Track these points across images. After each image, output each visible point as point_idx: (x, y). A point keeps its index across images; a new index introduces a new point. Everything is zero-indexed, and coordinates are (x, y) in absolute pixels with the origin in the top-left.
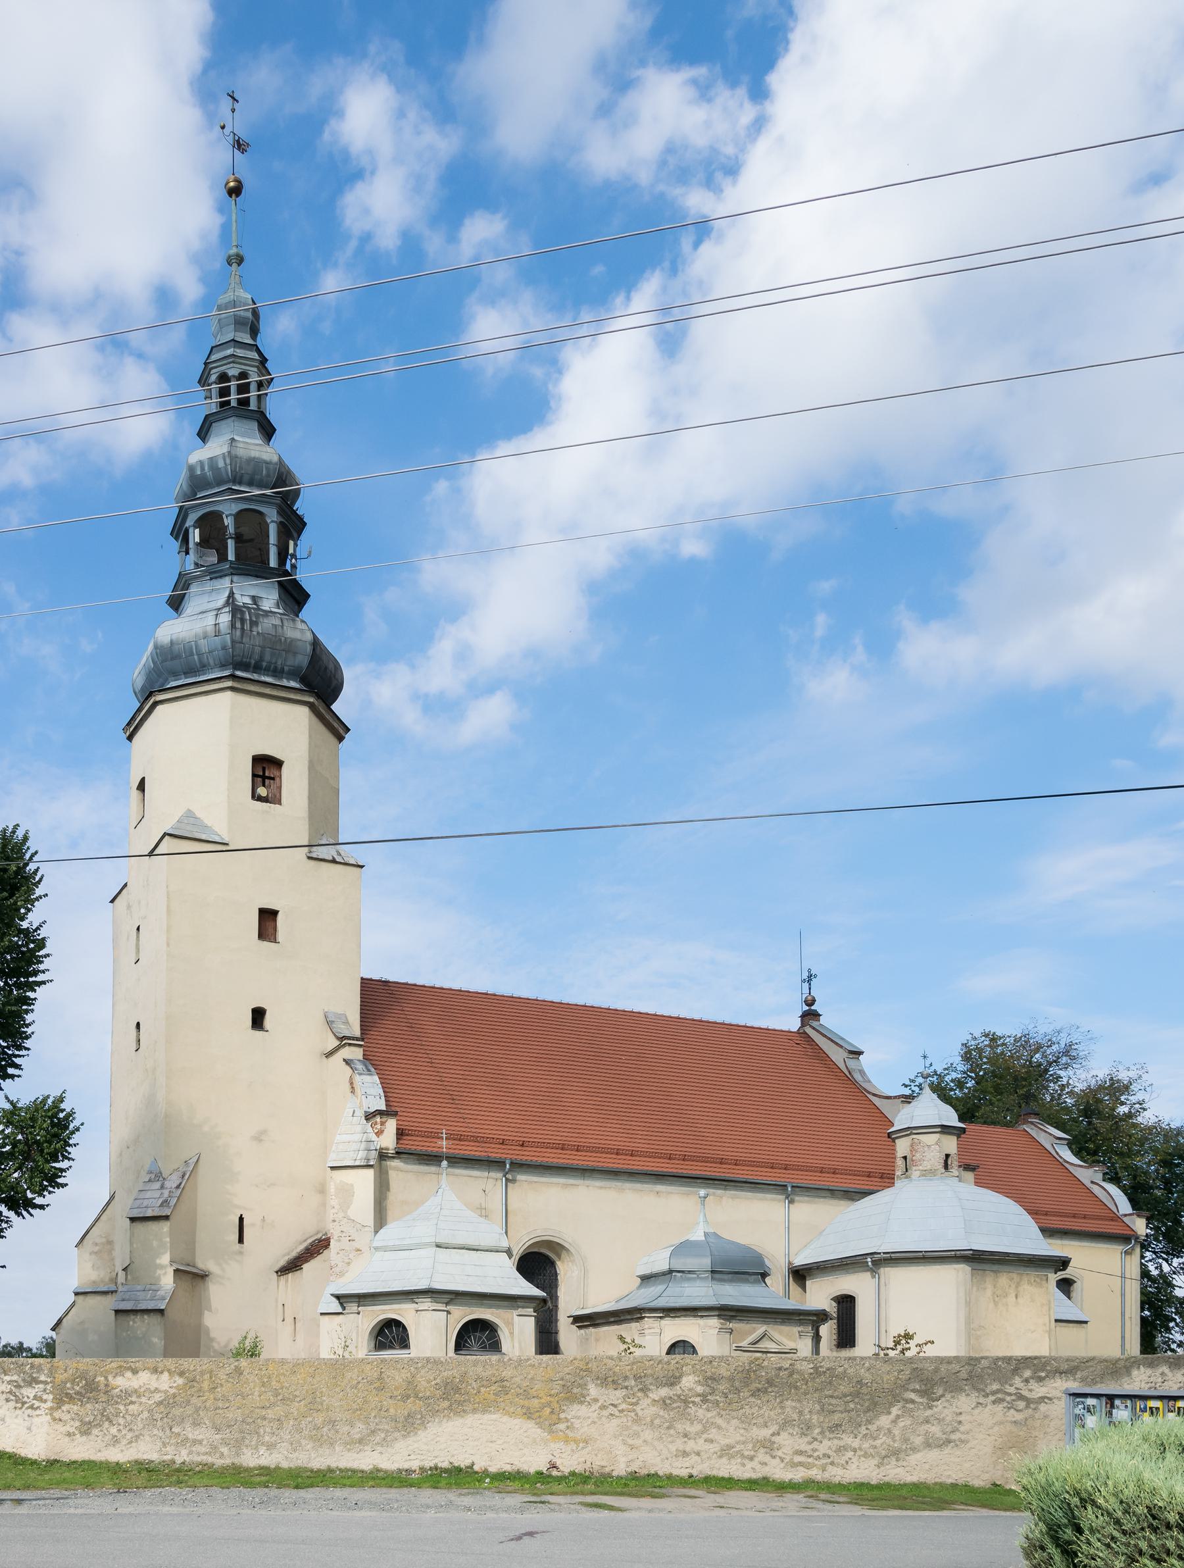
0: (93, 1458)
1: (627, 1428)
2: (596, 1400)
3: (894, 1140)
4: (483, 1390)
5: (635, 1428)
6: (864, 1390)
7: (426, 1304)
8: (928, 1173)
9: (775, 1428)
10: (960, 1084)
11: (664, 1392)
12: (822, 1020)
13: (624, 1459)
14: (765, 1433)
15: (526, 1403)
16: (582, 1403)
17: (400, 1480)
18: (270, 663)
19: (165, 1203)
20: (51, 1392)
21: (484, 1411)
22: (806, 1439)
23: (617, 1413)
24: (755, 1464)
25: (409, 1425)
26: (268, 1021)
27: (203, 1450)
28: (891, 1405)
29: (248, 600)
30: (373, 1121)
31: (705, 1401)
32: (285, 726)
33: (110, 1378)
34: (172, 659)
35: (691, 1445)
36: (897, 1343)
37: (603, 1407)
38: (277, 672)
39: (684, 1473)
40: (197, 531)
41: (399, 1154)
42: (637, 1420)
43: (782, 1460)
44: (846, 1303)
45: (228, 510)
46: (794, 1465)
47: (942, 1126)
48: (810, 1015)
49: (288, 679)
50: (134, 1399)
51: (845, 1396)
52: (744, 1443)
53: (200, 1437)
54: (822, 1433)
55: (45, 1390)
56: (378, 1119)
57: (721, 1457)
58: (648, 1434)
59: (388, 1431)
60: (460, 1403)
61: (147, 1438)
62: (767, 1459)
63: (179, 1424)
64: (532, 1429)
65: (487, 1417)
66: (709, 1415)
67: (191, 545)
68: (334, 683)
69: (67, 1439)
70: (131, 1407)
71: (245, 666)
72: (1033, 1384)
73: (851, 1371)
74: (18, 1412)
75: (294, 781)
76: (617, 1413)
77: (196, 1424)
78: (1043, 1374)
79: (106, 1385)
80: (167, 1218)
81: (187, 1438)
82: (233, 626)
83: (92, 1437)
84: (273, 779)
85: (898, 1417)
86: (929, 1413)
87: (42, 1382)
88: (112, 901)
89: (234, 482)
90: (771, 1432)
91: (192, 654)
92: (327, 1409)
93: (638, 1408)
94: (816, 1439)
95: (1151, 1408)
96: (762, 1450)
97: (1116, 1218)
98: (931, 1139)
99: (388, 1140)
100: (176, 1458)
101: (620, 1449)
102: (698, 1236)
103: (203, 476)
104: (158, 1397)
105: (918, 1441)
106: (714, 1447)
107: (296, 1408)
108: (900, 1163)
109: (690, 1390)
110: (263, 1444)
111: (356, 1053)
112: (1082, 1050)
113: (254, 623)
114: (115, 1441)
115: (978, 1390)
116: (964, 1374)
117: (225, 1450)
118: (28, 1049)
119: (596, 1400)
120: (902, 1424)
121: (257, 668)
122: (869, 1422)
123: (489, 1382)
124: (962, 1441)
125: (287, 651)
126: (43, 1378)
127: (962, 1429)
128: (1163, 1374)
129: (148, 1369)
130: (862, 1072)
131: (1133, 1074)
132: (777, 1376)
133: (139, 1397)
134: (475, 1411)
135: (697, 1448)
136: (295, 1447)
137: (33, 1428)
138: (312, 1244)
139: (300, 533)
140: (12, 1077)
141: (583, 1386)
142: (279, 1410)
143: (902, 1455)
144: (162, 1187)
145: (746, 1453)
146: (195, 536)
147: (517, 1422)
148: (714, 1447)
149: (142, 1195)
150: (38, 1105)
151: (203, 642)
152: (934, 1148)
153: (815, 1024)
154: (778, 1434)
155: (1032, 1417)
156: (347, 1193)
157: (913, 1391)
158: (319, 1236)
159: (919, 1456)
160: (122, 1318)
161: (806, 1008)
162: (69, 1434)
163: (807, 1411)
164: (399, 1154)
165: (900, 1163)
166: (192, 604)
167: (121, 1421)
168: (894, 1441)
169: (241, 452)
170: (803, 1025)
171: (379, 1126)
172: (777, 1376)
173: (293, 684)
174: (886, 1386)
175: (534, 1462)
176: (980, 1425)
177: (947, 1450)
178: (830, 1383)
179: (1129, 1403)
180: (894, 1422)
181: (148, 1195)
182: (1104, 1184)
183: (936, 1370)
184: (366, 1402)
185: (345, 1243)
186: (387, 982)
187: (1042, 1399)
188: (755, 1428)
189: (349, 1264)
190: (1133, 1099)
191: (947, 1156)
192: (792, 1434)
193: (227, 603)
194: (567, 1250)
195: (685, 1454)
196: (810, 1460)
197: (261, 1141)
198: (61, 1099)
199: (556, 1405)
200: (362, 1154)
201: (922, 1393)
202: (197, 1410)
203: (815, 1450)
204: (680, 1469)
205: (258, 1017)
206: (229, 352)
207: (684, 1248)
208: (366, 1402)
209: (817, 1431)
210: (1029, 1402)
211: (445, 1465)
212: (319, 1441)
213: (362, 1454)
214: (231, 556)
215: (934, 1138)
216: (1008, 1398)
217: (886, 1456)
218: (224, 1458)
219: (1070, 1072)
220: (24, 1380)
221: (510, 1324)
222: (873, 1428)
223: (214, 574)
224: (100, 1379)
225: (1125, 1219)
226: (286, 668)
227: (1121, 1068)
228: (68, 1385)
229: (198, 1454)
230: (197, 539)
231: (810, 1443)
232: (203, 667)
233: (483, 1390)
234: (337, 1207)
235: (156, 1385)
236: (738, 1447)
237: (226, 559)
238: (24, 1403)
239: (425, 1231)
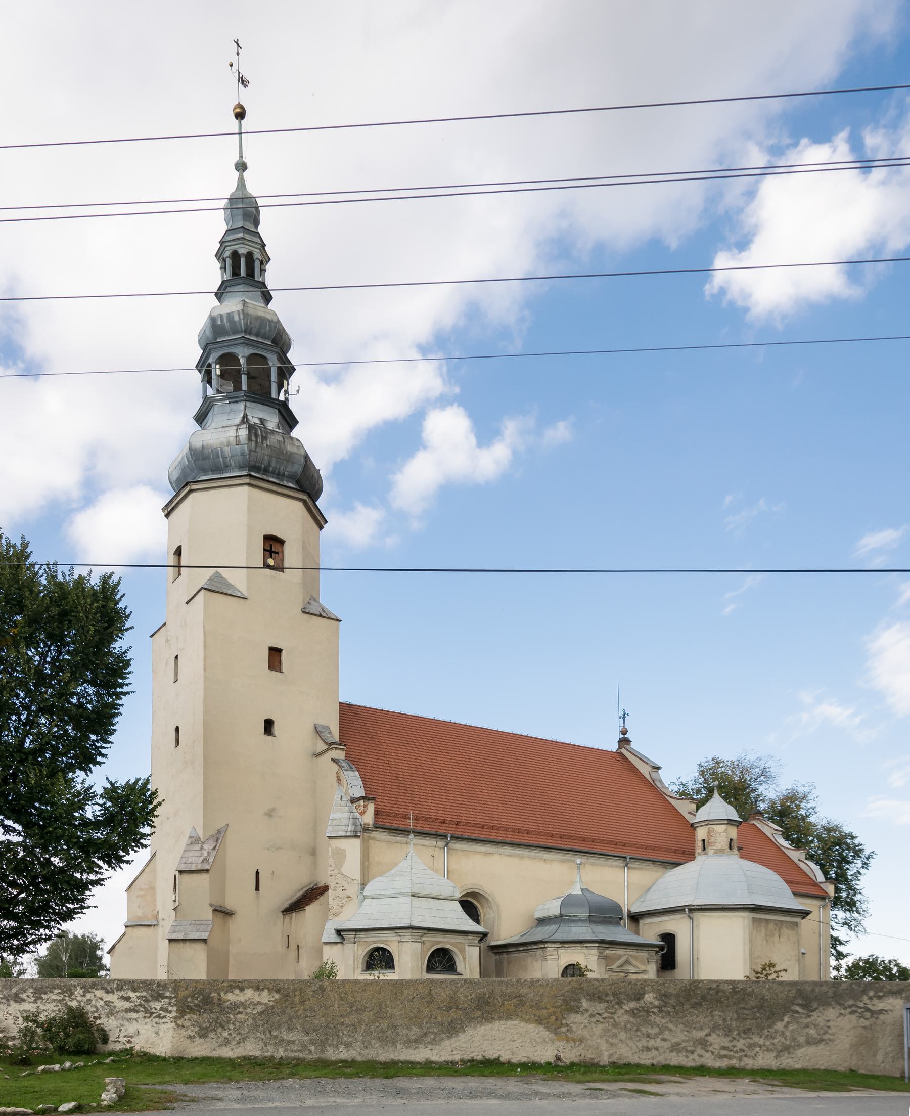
0: (209, 1055)
1: (609, 1030)
2: (587, 1010)
3: (695, 829)
4: (506, 1003)
5: (614, 1030)
6: (766, 1004)
7: (407, 936)
8: (719, 852)
9: (707, 1031)
10: (698, 791)
11: (633, 1005)
12: (633, 745)
13: (606, 1053)
14: (702, 1034)
15: (537, 1012)
16: (577, 1013)
17: (448, 1069)
18: (275, 468)
19: (205, 860)
20: (175, 1005)
21: (508, 1019)
22: (729, 1038)
23: (602, 1020)
24: (695, 1056)
25: (452, 1029)
26: (276, 729)
27: (296, 1048)
28: (784, 1015)
29: (257, 421)
30: (357, 804)
31: (660, 1011)
32: (283, 513)
33: (222, 994)
34: (204, 459)
35: (652, 1043)
36: (764, 969)
37: (592, 1016)
38: (280, 475)
39: (648, 1062)
40: (218, 366)
41: (376, 827)
42: (616, 1025)
43: (713, 1053)
44: (669, 939)
45: (242, 353)
46: (721, 1057)
47: (729, 820)
48: (624, 741)
49: (288, 482)
50: (241, 1010)
51: (753, 1008)
52: (687, 1041)
53: (293, 1038)
54: (739, 1034)
55: (170, 1003)
56: (362, 802)
57: (672, 1051)
58: (623, 1035)
59: (436, 1033)
60: (489, 1012)
61: (252, 1040)
62: (703, 1052)
63: (276, 1029)
64: (542, 1032)
65: (509, 1023)
66: (664, 1021)
67: (214, 376)
68: (317, 487)
69: (188, 1041)
70: (239, 1016)
71: (257, 469)
72: (875, 1001)
73: (757, 990)
74: (147, 1020)
75: (291, 555)
76: (602, 1020)
77: (290, 1029)
78: (881, 994)
79: (219, 1000)
80: (207, 871)
81: (283, 1040)
82: (250, 439)
83: (209, 1039)
84: (277, 553)
85: (788, 1023)
86: (809, 1020)
87: (167, 997)
88: (151, 636)
89: (246, 332)
90: (705, 1033)
91: (218, 457)
92: (391, 1017)
93: (615, 1017)
94: (735, 1039)
96: (700, 1047)
97: (815, 884)
98: (721, 828)
99: (369, 818)
100: (275, 1054)
101: (604, 1046)
102: (577, 891)
103: (223, 326)
104: (260, 1008)
105: (802, 1040)
106: (667, 1045)
107: (366, 1017)
108: (699, 844)
109: (650, 1003)
110: (342, 1043)
111: (340, 755)
112: (773, 770)
113: (264, 438)
114: (227, 1042)
115: (840, 1004)
116: (830, 994)
117: (313, 1048)
118: (112, 743)
119: (587, 1010)
120: (791, 1028)
121: (266, 471)
122: (770, 1027)
123: (511, 998)
124: (830, 1040)
126: (168, 994)
127: (830, 1031)
129: (252, 987)
130: (661, 781)
131: (806, 789)
132: (708, 993)
133: (245, 1008)
134: (500, 1018)
135: (657, 1045)
136: (367, 1045)
137: (161, 1033)
138: (307, 892)
139: (290, 375)
140: (100, 763)
141: (578, 1000)
142: (354, 1018)
143: (791, 1050)
144: (202, 848)
145: (689, 1048)
146: (217, 370)
147: (532, 1027)
148: (667, 1045)
149: (187, 854)
150: (130, 788)
151: (227, 450)
152: (723, 835)
153: (628, 747)
154: (710, 1035)
155: (875, 1024)
156: (340, 855)
157: (798, 1005)
158: (312, 886)
159: (802, 1050)
160: (174, 945)
161: (622, 736)
162: (190, 1037)
163: (728, 1018)
164: (376, 827)
165: (699, 844)
166: (215, 420)
167: (231, 1027)
168: (786, 1039)
169: (251, 311)
170: (620, 748)
171: (362, 808)
172: (708, 993)
173: (291, 485)
174: (780, 1001)
175: (545, 1054)
176: (842, 1029)
177: (821, 1046)
178: (744, 999)
180: (786, 1026)
181: (191, 854)
182: (806, 861)
183: (813, 991)
184: (419, 1011)
185: (339, 892)
186: (351, 705)
187: (881, 1011)
188: (694, 1031)
189: (342, 907)
190: (809, 806)
191: (731, 840)
192: (719, 1035)
193: (243, 422)
194: (487, 899)
195: (648, 1049)
196: (731, 1053)
197: (271, 816)
198: (147, 782)
199: (558, 1014)
200: (351, 828)
201: (803, 1006)
202: (291, 1018)
203: (734, 1046)
204: (646, 1059)
205: (269, 725)
206: (240, 235)
207: (568, 901)
208: (419, 1011)
209: (735, 1033)
210: (872, 1013)
211: (479, 1058)
212: (384, 1040)
213: (417, 1051)
214: (244, 387)
215: (724, 827)
216: (860, 1011)
217: (781, 1051)
218: (313, 1053)
219: (765, 786)
220: (151, 996)
221: (463, 951)
222: (771, 1030)
223: (232, 399)
224: (214, 995)
225: (822, 885)
226: (286, 473)
227: (799, 785)
228: (189, 1000)
229: (292, 1051)
230: (218, 372)
231: (731, 1041)
232: (226, 467)
233: (506, 1003)
234: (333, 865)
235: (258, 999)
236: (683, 1045)
237: (241, 389)
238: (152, 1014)
239: (402, 884)
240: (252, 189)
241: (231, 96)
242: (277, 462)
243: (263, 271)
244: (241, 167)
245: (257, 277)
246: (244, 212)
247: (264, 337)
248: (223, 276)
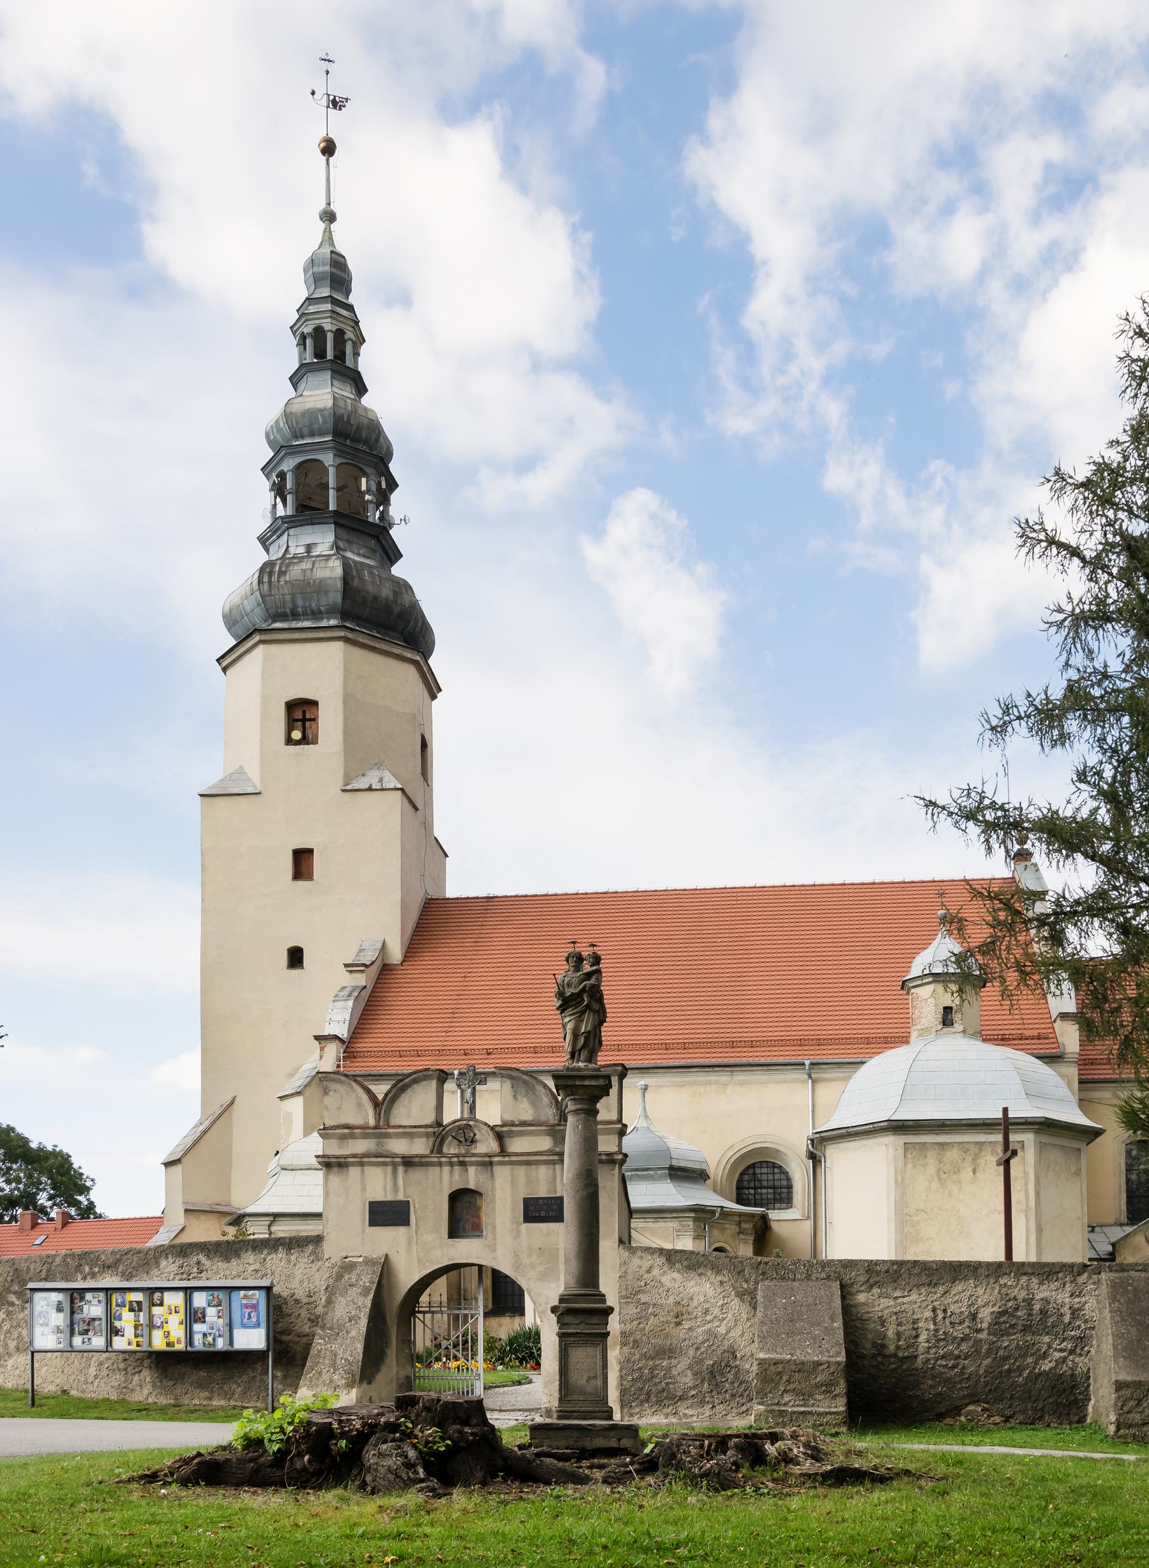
18: (304, 607)
38: (316, 615)
71: (281, 617)
95: (131, 1302)
121: (295, 616)
125: (318, 592)
128: (198, 1263)
173: (333, 622)
179: (102, 1296)
226: (322, 609)
240: (340, 248)
241: (318, 123)
242: (304, 599)
243: (356, 354)
244: (329, 217)
245: (349, 362)
246: (333, 276)
247: (322, 434)
248: (301, 358)
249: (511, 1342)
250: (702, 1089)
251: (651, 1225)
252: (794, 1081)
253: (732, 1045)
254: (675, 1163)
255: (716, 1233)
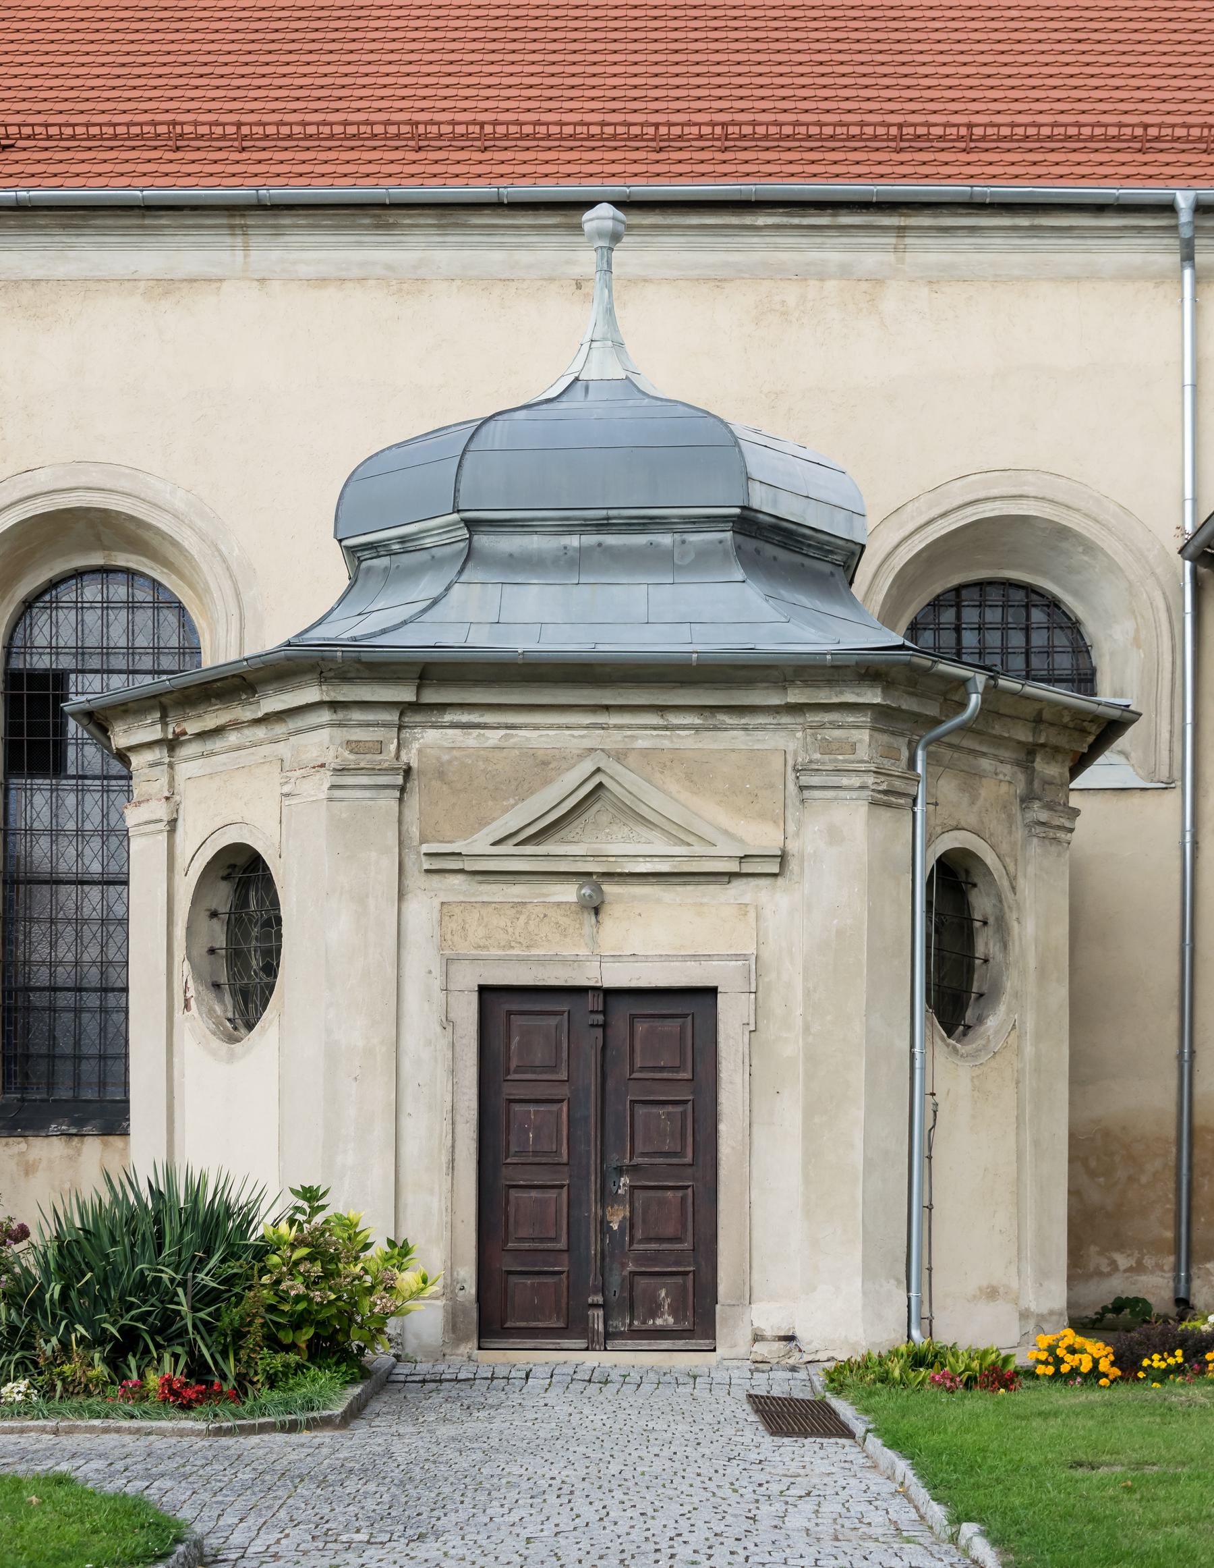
249: (71, 1253)
250: (791, 293)
251: (686, 741)
252: (1126, 276)
253: (903, 141)
254: (761, 500)
255: (948, 788)
